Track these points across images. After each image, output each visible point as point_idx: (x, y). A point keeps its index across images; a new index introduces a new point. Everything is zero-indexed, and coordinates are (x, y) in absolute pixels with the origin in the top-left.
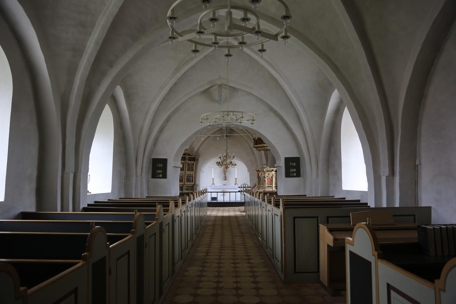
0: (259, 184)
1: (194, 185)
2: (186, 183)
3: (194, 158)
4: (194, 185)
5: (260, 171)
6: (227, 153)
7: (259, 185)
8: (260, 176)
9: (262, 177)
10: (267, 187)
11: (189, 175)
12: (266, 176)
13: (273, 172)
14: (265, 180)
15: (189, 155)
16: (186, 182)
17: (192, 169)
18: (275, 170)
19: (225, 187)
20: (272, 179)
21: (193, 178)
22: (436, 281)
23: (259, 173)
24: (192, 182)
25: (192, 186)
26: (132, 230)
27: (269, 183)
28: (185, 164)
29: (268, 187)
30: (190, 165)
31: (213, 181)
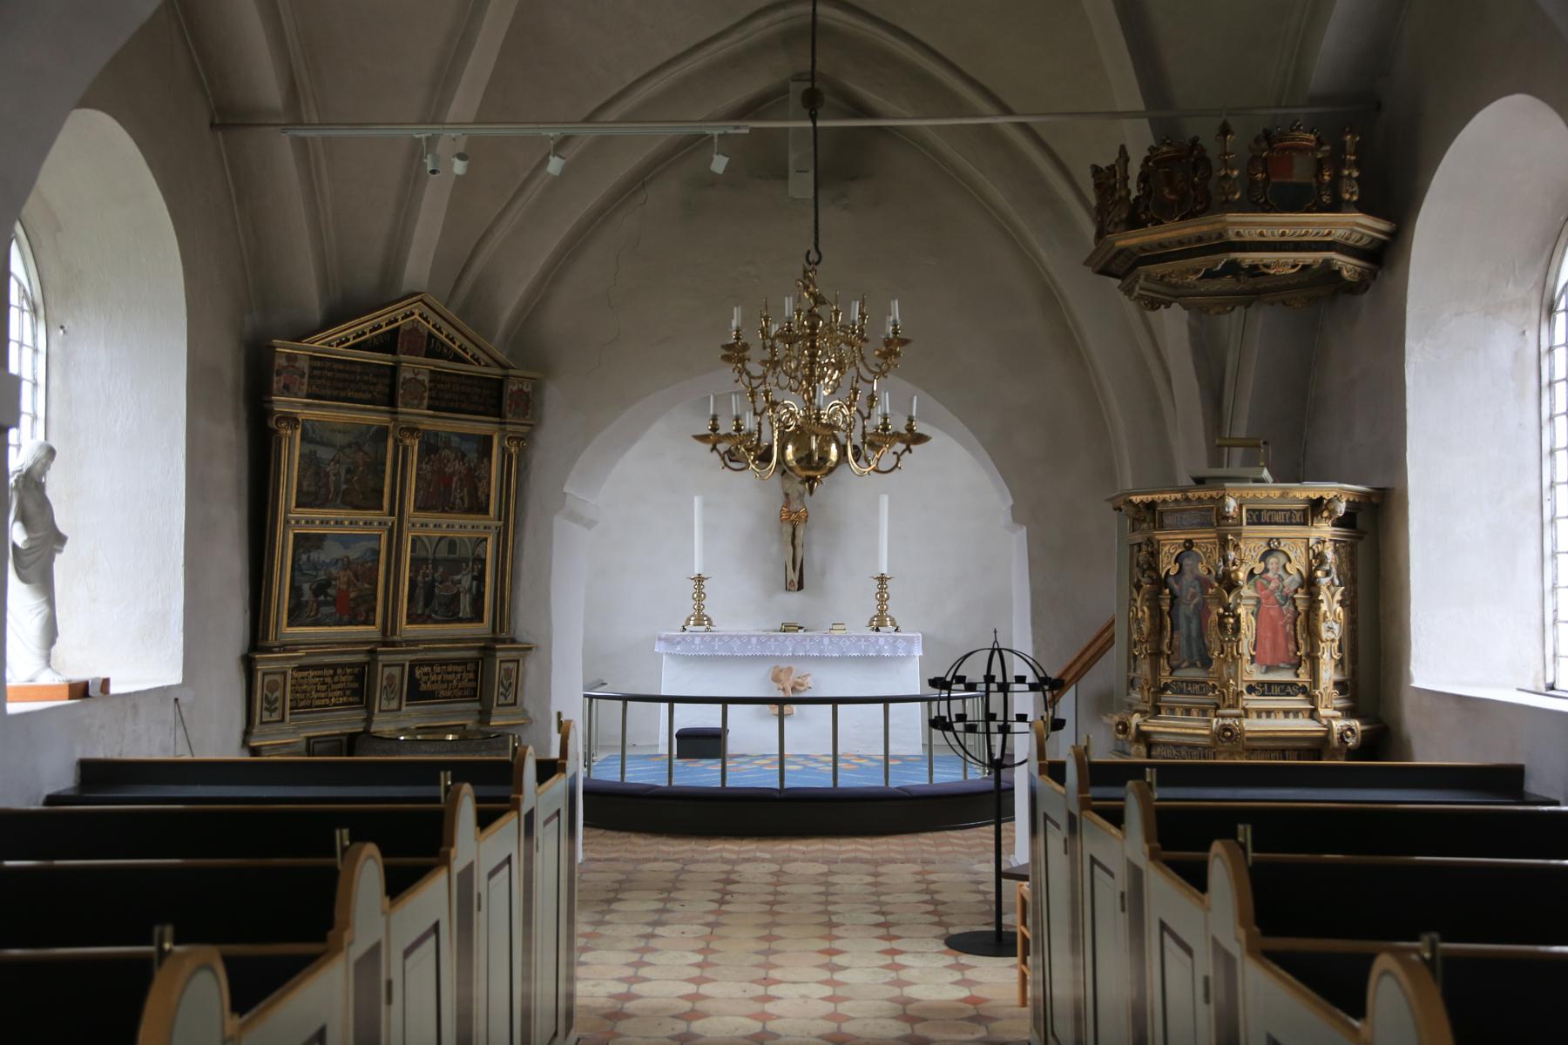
0: (1156, 654)
1: (488, 649)
2: (407, 630)
3: (498, 385)
4: (488, 649)
5: (1168, 520)
6: (818, 300)
7: (1155, 669)
8: (1168, 566)
9: (1187, 578)
10: (1251, 689)
12: (1242, 575)
13: (1324, 530)
14: (1237, 618)
15: (430, 354)
16: (412, 619)
17: (474, 490)
18: (1341, 508)
19: (790, 644)
20: (1313, 603)
21: (480, 578)
23: (1160, 536)
24: (477, 616)
25: (475, 661)
27: (1274, 645)
28: (396, 441)
29: (1266, 689)
30: (445, 452)
31: (700, 596)
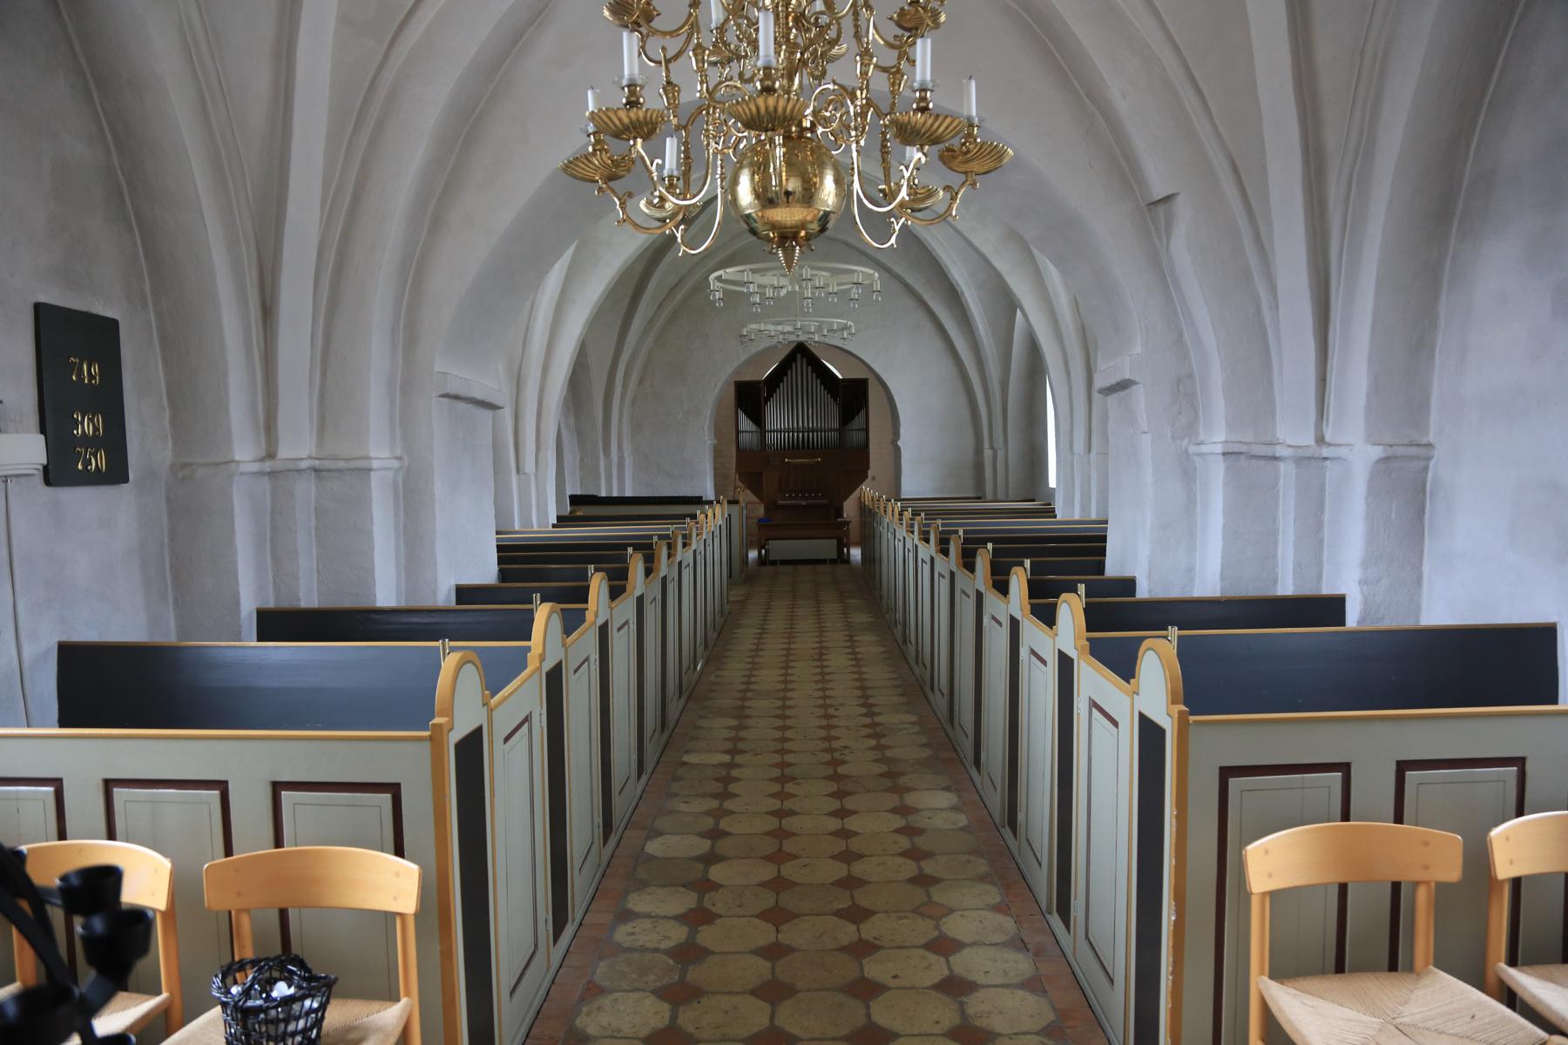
11: (238, 975)
22: (1132, 681)
26: (1057, 265)
